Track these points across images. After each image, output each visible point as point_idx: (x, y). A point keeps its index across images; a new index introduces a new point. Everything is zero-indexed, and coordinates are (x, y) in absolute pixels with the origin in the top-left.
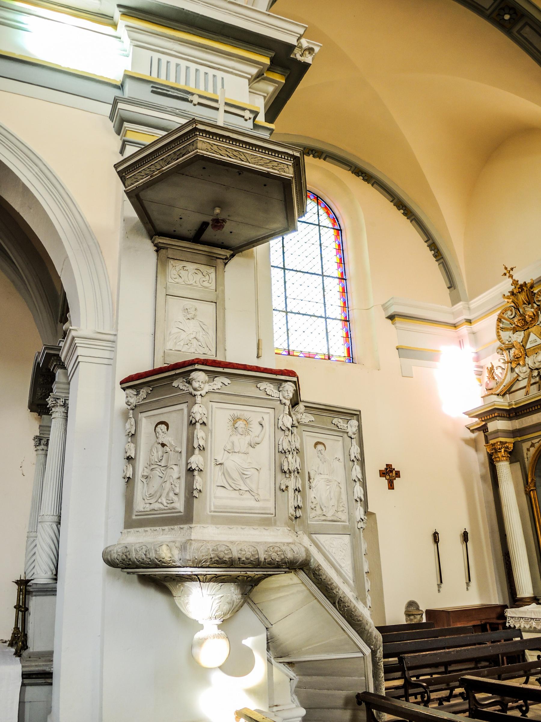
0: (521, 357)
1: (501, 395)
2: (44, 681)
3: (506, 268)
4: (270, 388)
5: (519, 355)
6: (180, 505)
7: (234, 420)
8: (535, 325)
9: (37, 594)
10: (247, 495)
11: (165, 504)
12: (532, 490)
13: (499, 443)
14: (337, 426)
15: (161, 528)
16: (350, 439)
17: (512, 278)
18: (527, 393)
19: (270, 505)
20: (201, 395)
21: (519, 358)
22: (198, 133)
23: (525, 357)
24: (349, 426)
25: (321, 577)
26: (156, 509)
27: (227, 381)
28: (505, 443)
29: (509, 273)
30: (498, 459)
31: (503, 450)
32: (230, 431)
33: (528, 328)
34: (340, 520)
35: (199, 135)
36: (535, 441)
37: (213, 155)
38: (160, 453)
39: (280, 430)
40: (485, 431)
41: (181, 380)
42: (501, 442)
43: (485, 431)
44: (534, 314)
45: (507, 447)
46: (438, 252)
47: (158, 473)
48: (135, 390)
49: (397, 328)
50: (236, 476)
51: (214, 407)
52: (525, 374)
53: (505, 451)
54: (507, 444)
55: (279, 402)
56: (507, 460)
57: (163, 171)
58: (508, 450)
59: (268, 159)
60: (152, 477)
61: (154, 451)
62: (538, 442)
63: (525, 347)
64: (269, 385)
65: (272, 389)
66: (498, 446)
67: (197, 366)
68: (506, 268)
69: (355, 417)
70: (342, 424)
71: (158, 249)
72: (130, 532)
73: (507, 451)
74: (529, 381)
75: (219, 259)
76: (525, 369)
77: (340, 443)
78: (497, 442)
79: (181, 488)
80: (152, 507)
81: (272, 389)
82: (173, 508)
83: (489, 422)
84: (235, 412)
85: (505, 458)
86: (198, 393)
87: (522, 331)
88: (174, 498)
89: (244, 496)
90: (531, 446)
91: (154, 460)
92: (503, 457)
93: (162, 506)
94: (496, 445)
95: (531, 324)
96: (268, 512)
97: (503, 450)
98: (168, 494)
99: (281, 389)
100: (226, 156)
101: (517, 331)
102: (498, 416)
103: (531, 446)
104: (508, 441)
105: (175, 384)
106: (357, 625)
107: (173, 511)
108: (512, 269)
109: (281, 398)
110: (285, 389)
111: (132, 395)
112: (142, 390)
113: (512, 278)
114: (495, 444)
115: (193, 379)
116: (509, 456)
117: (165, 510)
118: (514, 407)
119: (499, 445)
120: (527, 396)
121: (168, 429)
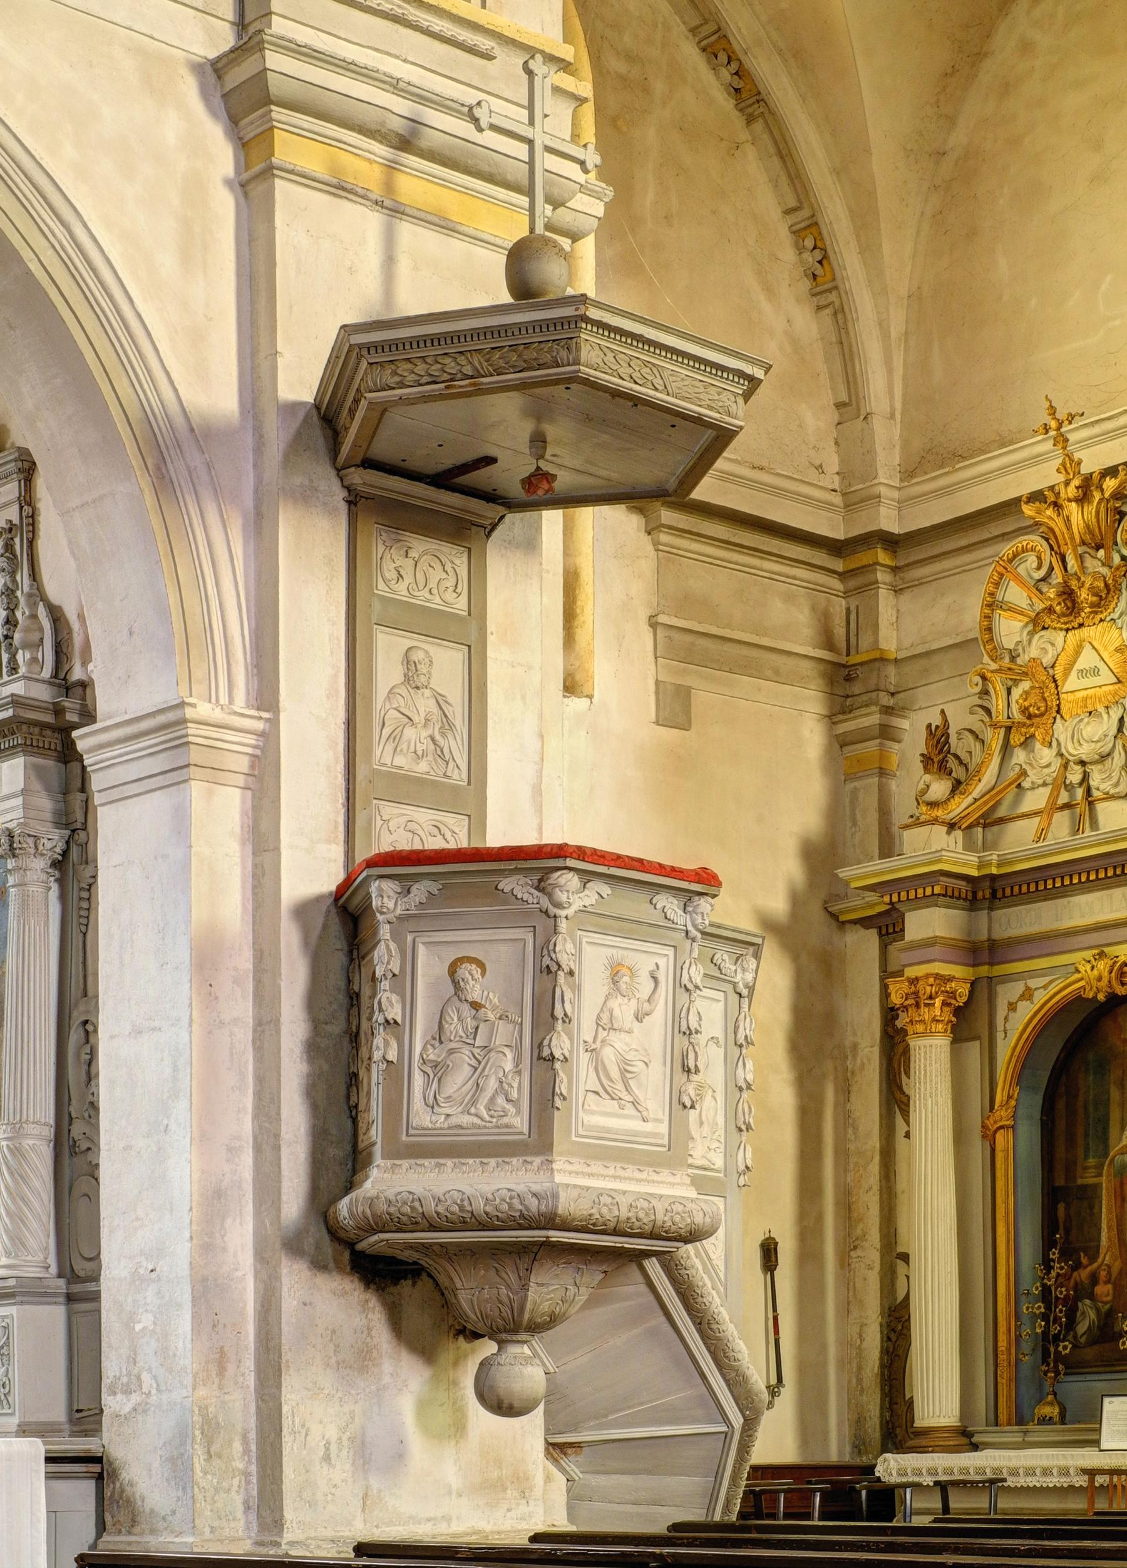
0: (1042, 715)
1: (960, 828)
2: (84, 1469)
3: (1053, 411)
4: (670, 904)
5: (1038, 709)
6: (519, 1121)
7: (611, 967)
8: (1101, 620)
9: (24, 1299)
10: (630, 1110)
11: (487, 1118)
12: (1002, 1127)
13: (931, 980)
14: (719, 969)
15: (478, 1160)
16: (737, 997)
17: (1064, 448)
18: (1041, 835)
19: (664, 1128)
20: (566, 917)
21: (1036, 716)
22: (584, 325)
23: (1055, 718)
24: (739, 970)
25: (688, 1272)
26: (465, 1125)
27: (606, 890)
28: (949, 980)
29: (1058, 429)
30: (920, 1028)
31: (938, 1002)
32: (606, 987)
33: (1081, 625)
34: (712, 1167)
35: (586, 329)
36: (1033, 983)
37: (607, 377)
38: (470, 1023)
39: (683, 989)
40: (884, 932)
41: (522, 879)
42: (937, 976)
43: (884, 932)
44: (1106, 585)
45: (953, 994)
46: (825, 262)
47: (467, 1059)
48: (397, 882)
49: (661, 547)
50: (615, 1073)
51: (585, 940)
52: (1046, 771)
53: (944, 1004)
54: (953, 985)
55: (683, 934)
56: (946, 1031)
57: (483, 384)
58: (953, 1002)
59: (700, 381)
60: (451, 1065)
61: (452, 1015)
62: (1045, 987)
63: (1059, 683)
64: (671, 899)
65: (676, 909)
66: (928, 989)
67: (570, 863)
68: (1053, 411)
69: (751, 949)
70: (727, 965)
71: (354, 500)
72: (400, 1165)
73: (949, 1005)
74: (1054, 796)
75: (477, 526)
76: (1046, 755)
77: (721, 1005)
78: (927, 976)
79: (520, 1087)
80: (453, 1121)
81: (676, 909)
82: (507, 1126)
83: (910, 910)
84: (614, 951)
85: (940, 1027)
86: (563, 913)
87: (1061, 629)
88: (507, 1106)
89: (625, 1112)
90: (1023, 997)
91: (456, 1032)
92: (938, 1021)
93: (478, 1122)
94: (921, 983)
95: (1091, 613)
96: (660, 1142)
97: (938, 1002)
98: (492, 1099)
99: (690, 909)
100: (628, 379)
101: (1044, 628)
102: (943, 895)
103: (1023, 997)
104: (957, 976)
105: (506, 884)
106: (731, 1368)
107: (505, 1130)
108: (1071, 418)
109: (690, 928)
110: (699, 910)
111: (392, 894)
112: (416, 886)
113: (1064, 448)
114: (917, 979)
115: (556, 886)
116: (951, 1022)
117: (485, 1127)
118: (994, 871)
119: (932, 985)
120: (1039, 844)
121: (483, 973)
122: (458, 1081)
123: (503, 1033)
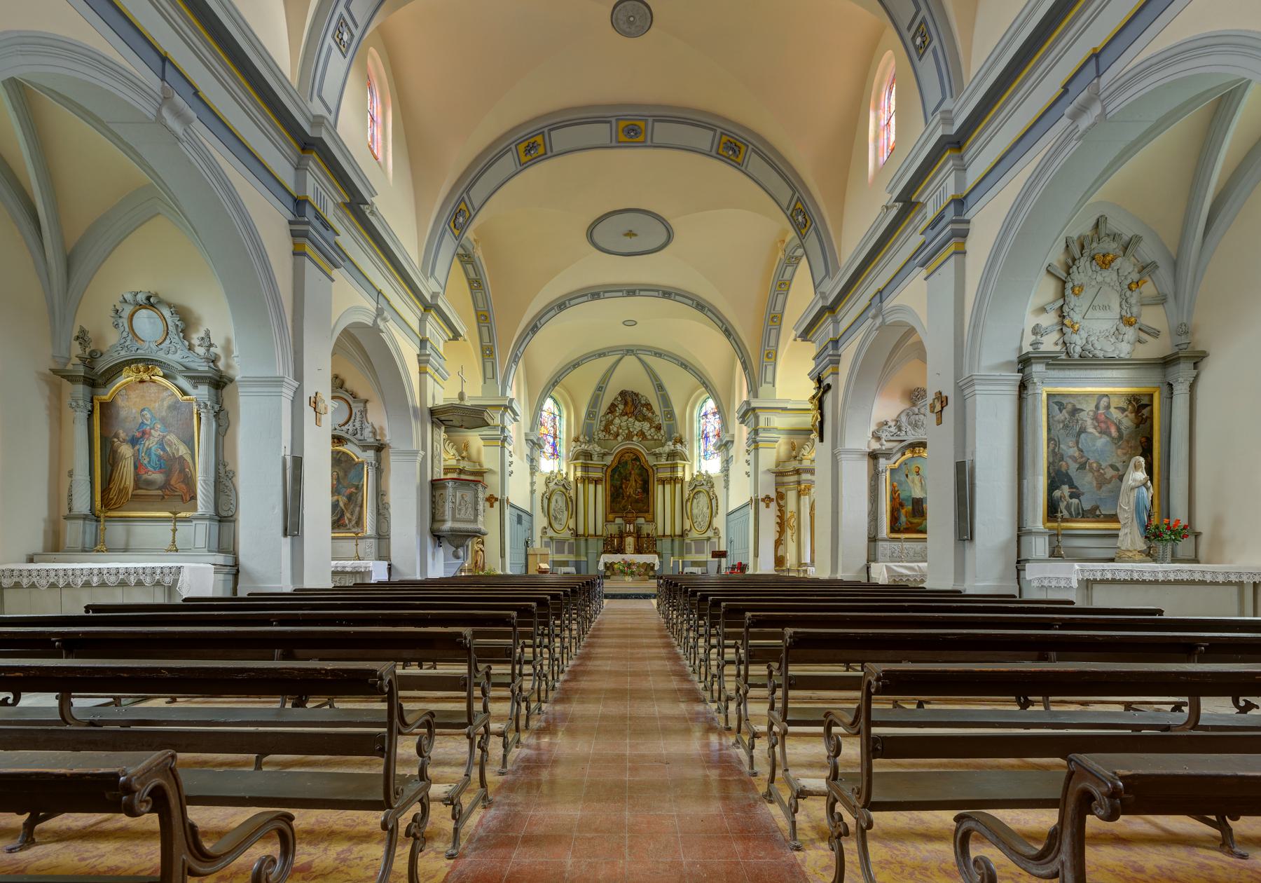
79: (472, 513)
122: (463, 512)
123: (470, 505)
